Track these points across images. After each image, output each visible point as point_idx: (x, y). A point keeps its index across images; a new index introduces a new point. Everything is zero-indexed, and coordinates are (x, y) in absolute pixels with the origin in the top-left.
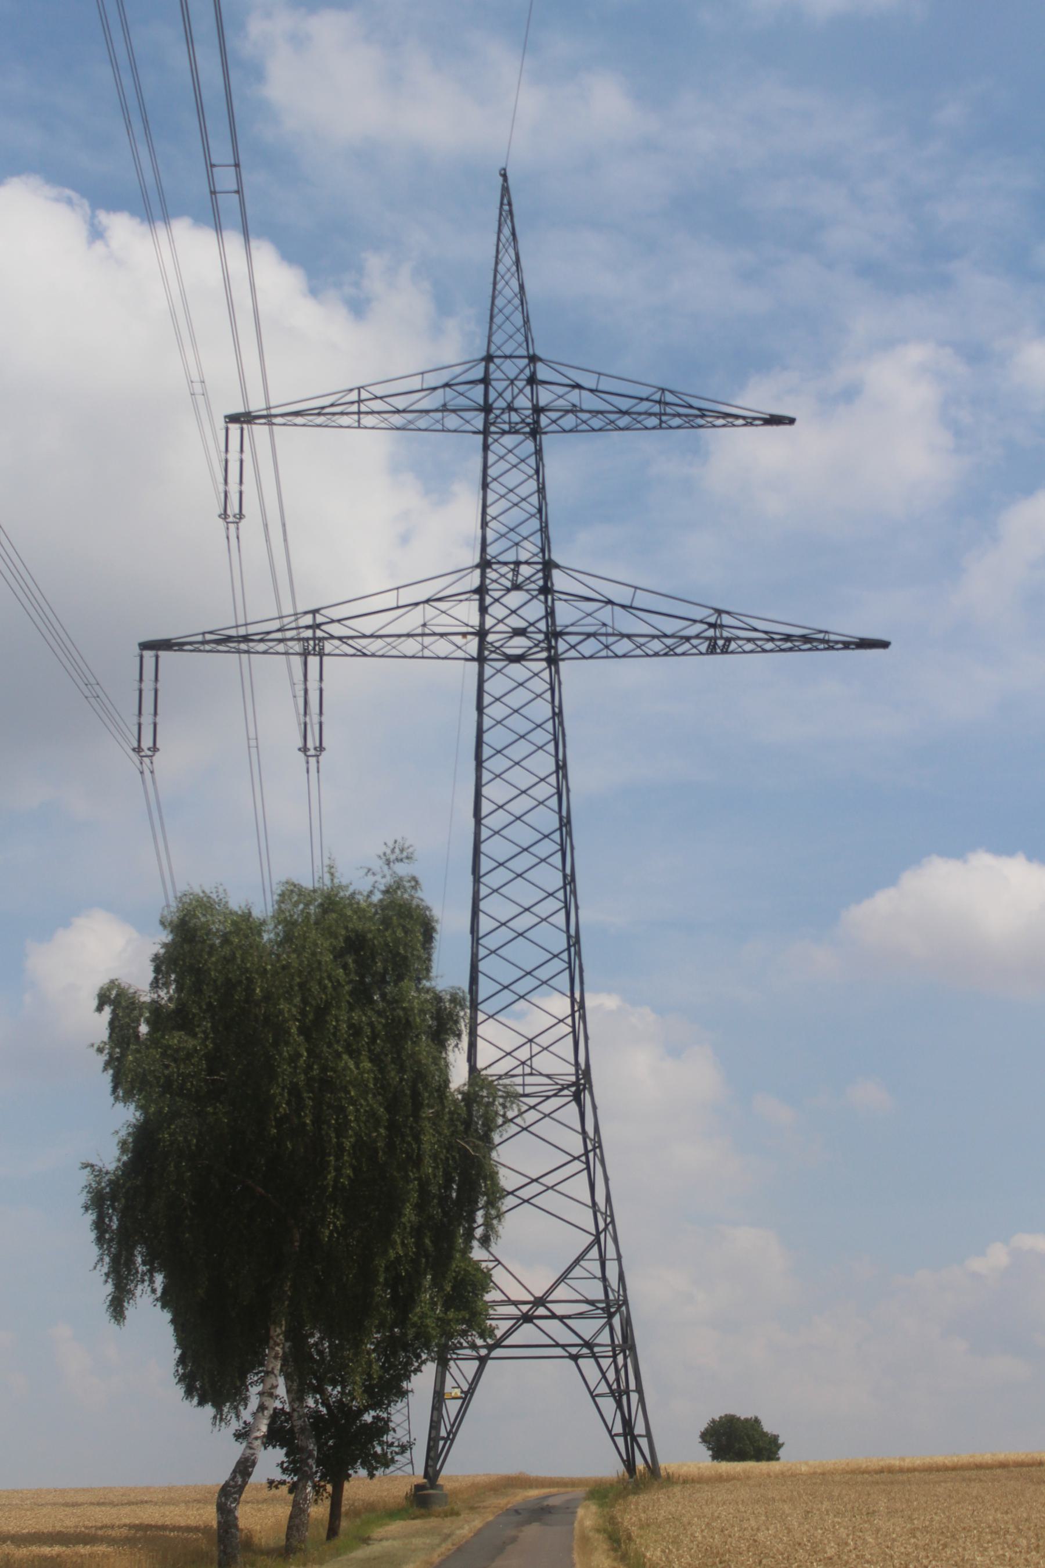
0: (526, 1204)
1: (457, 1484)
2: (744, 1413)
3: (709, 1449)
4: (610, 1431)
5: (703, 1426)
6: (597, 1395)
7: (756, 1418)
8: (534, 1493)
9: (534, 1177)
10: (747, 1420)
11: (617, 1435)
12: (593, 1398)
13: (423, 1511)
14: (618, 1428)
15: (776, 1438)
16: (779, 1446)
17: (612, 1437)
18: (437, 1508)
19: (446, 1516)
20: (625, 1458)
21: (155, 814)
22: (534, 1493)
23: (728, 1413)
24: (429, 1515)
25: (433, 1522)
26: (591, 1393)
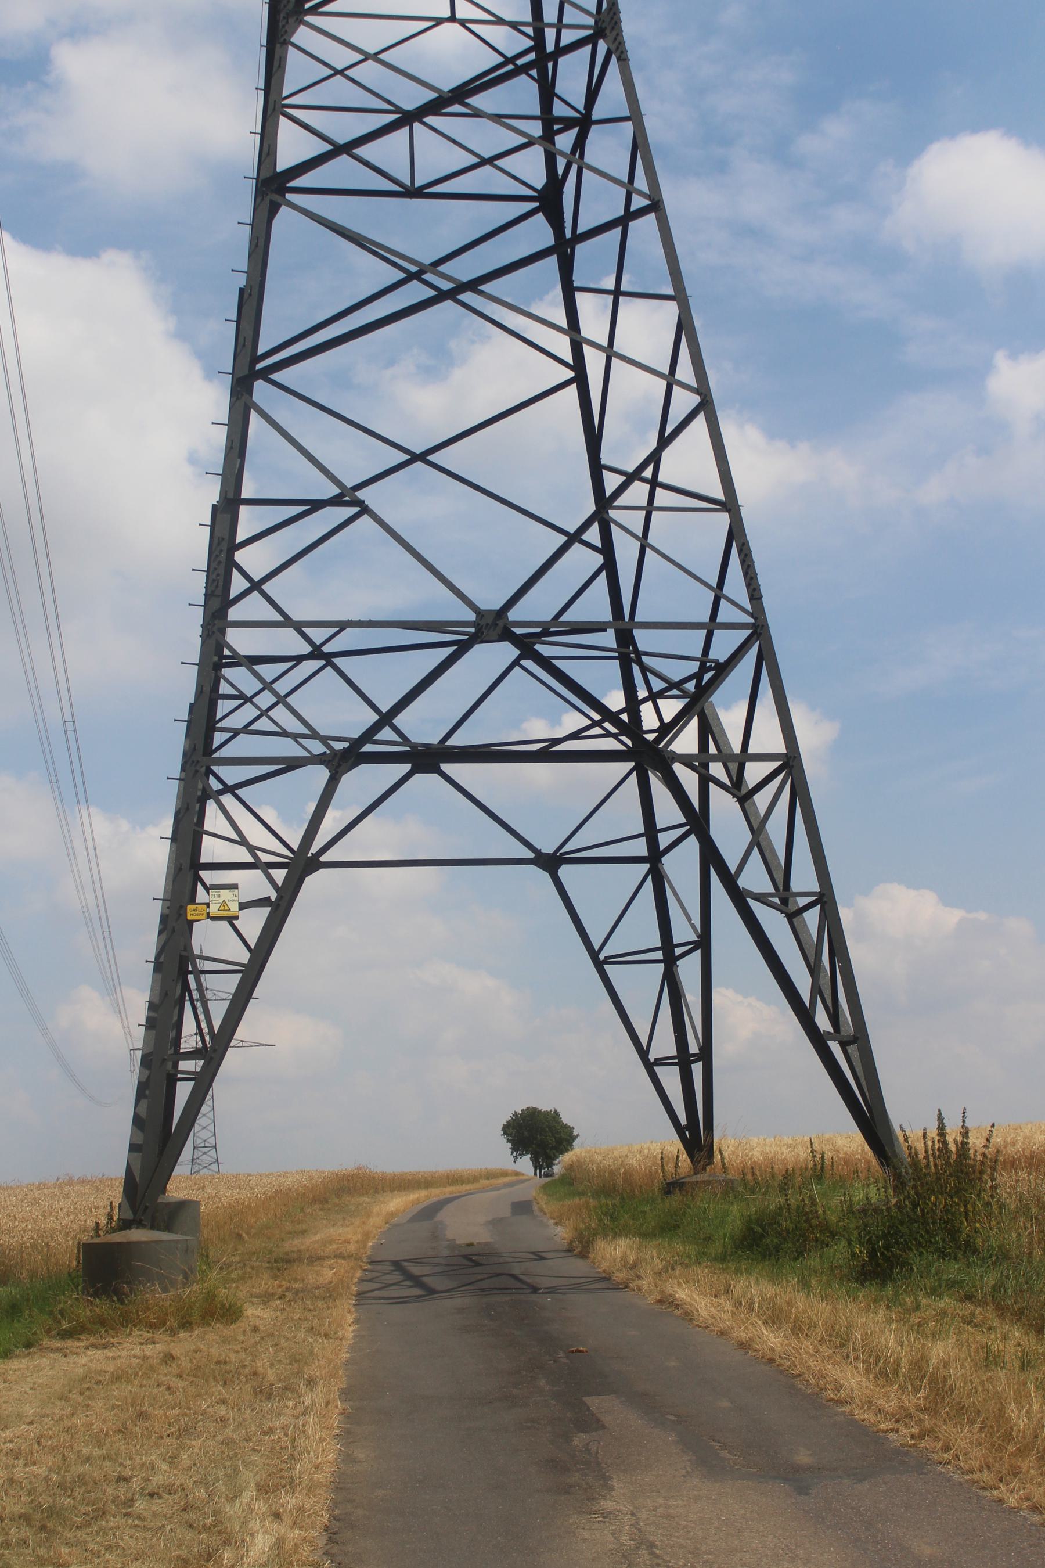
0: (419, 465)
1: (245, 1195)
2: (544, 1106)
3: (508, 1141)
4: (643, 1053)
5: (506, 1118)
6: (609, 960)
7: (556, 1111)
8: (396, 1203)
9: (487, 155)
10: (548, 1113)
11: (661, 1062)
12: (599, 966)
13: (102, 1307)
14: (664, 1045)
15: (570, 1129)
16: (574, 1138)
17: (650, 1067)
18: (155, 1296)
19: (186, 1324)
20: (683, 1121)
21: (20, 626)
22: (396, 1203)
23: (530, 1106)
24: (126, 1322)
25: (131, 1349)
26: (594, 954)
